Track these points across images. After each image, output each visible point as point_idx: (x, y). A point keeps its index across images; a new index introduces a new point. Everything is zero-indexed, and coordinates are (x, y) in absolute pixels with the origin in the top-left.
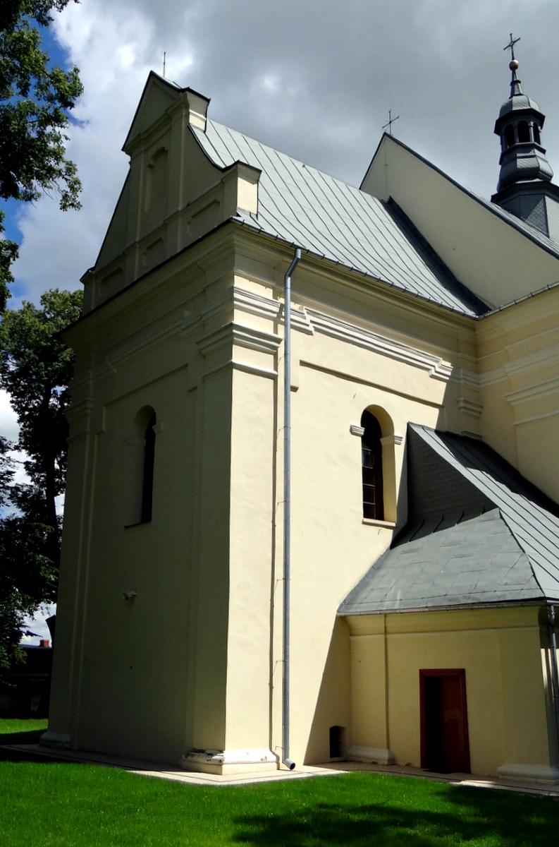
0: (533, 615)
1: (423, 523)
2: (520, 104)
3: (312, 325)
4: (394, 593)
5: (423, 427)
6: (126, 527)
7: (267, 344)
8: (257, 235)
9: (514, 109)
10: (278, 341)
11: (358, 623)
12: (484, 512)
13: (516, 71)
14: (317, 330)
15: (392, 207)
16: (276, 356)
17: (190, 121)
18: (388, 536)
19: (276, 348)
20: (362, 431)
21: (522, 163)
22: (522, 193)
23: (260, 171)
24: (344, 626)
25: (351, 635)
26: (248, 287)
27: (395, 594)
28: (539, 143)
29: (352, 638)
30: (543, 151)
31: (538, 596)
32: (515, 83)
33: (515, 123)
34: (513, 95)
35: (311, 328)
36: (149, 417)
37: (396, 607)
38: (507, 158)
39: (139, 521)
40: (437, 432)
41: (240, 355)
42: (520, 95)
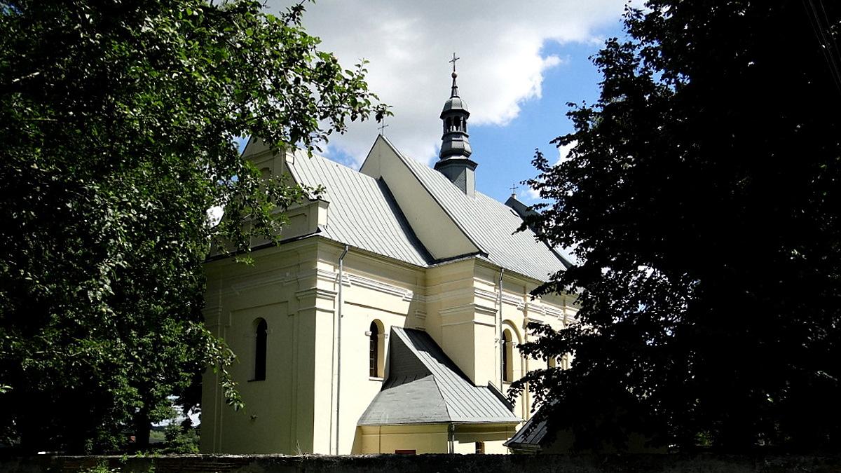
0: (446, 427)
1: (396, 380)
2: (456, 105)
3: (350, 282)
4: (385, 415)
5: (398, 328)
6: (249, 381)
7: (330, 295)
8: (330, 241)
9: (453, 108)
10: (336, 294)
11: (367, 429)
12: (426, 376)
13: (456, 79)
14: (352, 284)
15: (382, 183)
16: (334, 301)
17: (287, 159)
18: (380, 385)
19: (334, 297)
20: (370, 333)
21: (455, 145)
22: (454, 165)
23: (329, 203)
24: (359, 428)
25: (363, 434)
26: (323, 267)
27: (385, 416)
28: (465, 131)
29: (364, 436)
30: (467, 136)
31: (447, 420)
32: (454, 88)
33: (453, 117)
34: (452, 97)
35: (349, 284)
36: (261, 326)
37: (386, 423)
38: (447, 137)
39: (254, 378)
40: (404, 329)
41: (320, 303)
42: (457, 97)
